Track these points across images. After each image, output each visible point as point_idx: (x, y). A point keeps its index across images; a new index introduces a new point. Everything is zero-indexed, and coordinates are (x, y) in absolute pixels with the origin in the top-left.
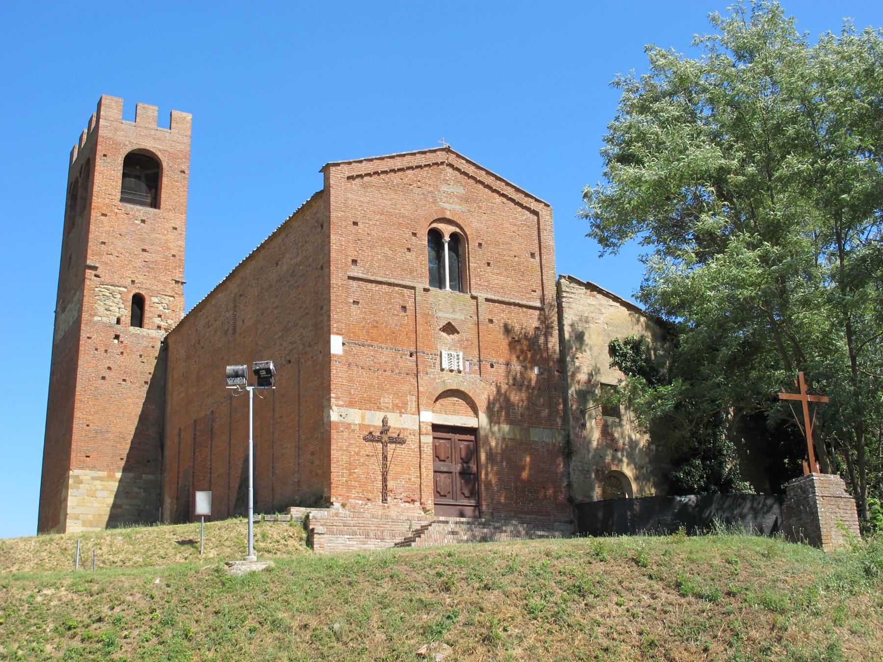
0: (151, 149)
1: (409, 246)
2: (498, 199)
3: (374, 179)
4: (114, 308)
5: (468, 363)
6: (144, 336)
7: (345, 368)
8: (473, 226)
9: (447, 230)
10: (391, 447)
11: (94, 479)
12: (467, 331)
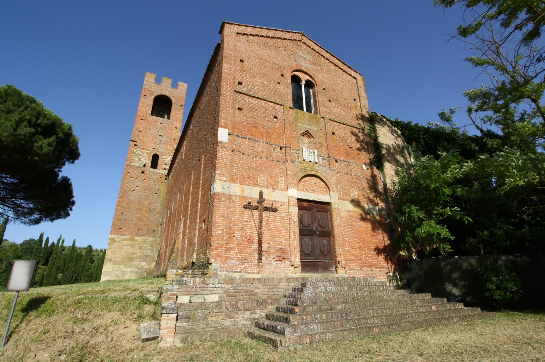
0: (169, 96)
1: (279, 81)
2: (333, 67)
3: (256, 39)
4: (143, 159)
5: (320, 158)
6: (157, 173)
7: (229, 152)
8: (320, 78)
9: (304, 78)
10: (266, 214)
11: (122, 240)
12: (319, 137)
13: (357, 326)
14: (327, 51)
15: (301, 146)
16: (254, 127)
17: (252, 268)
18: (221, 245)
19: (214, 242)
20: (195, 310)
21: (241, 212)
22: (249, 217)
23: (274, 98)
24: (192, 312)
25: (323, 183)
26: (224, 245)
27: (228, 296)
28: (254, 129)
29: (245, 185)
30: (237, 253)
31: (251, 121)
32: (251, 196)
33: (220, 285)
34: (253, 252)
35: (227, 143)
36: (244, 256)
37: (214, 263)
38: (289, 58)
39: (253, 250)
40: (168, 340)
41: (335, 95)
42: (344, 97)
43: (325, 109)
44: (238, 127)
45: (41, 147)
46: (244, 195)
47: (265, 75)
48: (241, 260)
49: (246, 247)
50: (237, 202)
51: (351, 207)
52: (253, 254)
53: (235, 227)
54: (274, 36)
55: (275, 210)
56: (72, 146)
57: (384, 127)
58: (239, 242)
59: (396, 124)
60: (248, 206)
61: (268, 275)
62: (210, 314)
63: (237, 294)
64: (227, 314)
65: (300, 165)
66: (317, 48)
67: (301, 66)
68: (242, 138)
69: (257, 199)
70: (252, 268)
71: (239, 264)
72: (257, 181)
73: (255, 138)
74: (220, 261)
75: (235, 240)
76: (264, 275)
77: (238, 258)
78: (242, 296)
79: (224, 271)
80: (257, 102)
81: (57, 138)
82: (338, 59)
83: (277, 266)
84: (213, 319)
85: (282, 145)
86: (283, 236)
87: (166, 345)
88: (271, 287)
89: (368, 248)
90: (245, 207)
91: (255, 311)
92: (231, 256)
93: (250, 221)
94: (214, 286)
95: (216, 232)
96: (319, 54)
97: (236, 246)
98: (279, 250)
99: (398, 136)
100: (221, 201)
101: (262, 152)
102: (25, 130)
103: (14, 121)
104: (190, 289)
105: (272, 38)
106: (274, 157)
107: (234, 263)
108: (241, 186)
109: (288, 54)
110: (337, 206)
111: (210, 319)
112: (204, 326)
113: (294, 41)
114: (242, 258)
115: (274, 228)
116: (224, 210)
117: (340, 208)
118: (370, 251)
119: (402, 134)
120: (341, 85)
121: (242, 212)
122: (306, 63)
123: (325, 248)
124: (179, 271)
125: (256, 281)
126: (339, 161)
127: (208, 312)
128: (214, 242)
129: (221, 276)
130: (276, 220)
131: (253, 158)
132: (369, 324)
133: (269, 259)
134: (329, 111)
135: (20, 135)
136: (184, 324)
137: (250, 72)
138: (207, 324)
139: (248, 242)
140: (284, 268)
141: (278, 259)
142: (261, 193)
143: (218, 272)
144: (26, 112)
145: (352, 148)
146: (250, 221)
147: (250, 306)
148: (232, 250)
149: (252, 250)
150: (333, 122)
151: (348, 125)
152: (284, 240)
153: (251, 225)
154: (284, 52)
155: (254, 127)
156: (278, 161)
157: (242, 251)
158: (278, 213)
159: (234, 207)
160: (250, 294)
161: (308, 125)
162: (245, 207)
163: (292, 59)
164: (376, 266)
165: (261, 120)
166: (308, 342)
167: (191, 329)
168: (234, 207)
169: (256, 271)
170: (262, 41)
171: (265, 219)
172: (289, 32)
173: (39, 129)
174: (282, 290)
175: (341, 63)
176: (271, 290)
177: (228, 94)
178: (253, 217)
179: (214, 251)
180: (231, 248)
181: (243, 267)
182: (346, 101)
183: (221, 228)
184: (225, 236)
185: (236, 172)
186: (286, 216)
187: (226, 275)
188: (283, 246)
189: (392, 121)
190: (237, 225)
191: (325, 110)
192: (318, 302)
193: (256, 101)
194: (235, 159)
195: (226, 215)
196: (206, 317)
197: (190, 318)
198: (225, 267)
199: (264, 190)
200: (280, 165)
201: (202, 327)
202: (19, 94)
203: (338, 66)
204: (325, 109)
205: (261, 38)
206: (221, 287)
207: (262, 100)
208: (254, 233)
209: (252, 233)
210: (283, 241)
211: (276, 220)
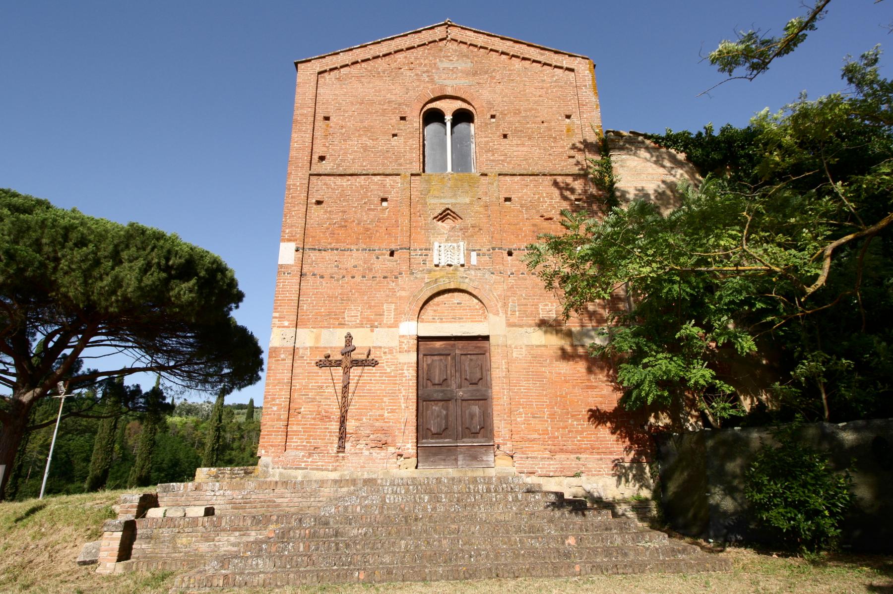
3: (354, 70)
5: (474, 254)
10: (355, 371)
13: (343, 565)
14: (502, 39)
15: (432, 239)
16: (343, 227)
17: (325, 462)
18: (277, 428)
19: (265, 425)
20: (160, 528)
21: (312, 373)
22: (326, 379)
23: (383, 165)
24: (155, 531)
25: (476, 301)
26: (280, 428)
27: (233, 508)
28: (341, 232)
29: (321, 327)
30: (302, 439)
31: (337, 218)
32: (331, 345)
33: (221, 492)
34: (330, 436)
35: (292, 266)
36: (314, 442)
37: (265, 455)
38: (419, 80)
39: (330, 432)
40: (108, 565)
41: (519, 122)
42: (539, 120)
43: (493, 155)
44: (314, 234)
45: (178, 296)
46: (319, 345)
47: (367, 129)
48: (309, 450)
49: (318, 429)
50: (307, 357)
51: (539, 337)
52: (330, 439)
53: (302, 399)
54: (388, 52)
55: (375, 364)
56: (223, 285)
57: (635, 154)
58: (306, 421)
59: (671, 141)
60: (326, 362)
61: (352, 473)
62: (179, 534)
63: (248, 505)
64: (204, 535)
65: (426, 276)
66: (481, 40)
67: (443, 87)
68: (319, 250)
69: (340, 347)
70: (325, 462)
71: (303, 456)
72: (344, 318)
73: (342, 246)
74: (273, 452)
75: (300, 419)
76: (346, 473)
77: (304, 446)
78: (255, 508)
79: (278, 468)
80: (349, 183)
81: (200, 278)
82: (529, 45)
83: (370, 458)
84: (183, 540)
85: (393, 247)
86: (387, 406)
87: (104, 571)
88: (304, 494)
89: (573, 416)
90: (320, 364)
91: (248, 532)
92: (293, 444)
93: (327, 387)
94: (213, 493)
95: (269, 408)
96: (486, 48)
97: (302, 428)
98: (376, 431)
99: (678, 164)
100: (279, 360)
101: (355, 267)
102: (152, 278)
103: (137, 270)
104: (179, 498)
105: (384, 56)
106: (377, 272)
107: (296, 456)
108: (315, 330)
109: (417, 75)
110: (501, 341)
111: (179, 541)
112: (170, 550)
113: (432, 44)
114: (311, 446)
115: (371, 393)
116: (283, 373)
117: (509, 343)
118: (578, 420)
119: (689, 158)
120: (535, 96)
121: (315, 373)
122: (456, 78)
123: (476, 419)
124: (212, 469)
125: (279, 484)
126: (515, 253)
127: (177, 531)
128: (265, 425)
129: (274, 476)
130: (375, 380)
131: (338, 280)
132: (370, 565)
133: (358, 447)
134: (502, 158)
135: (147, 286)
136: (144, 546)
137: (341, 133)
138: (175, 548)
139: (322, 419)
140: (383, 459)
141: (374, 445)
142: (349, 338)
143: (270, 470)
144: (154, 254)
145: (551, 219)
146: (327, 387)
147: (241, 524)
148: (294, 435)
149: (329, 432)
150: (508, 178)
151: (544, 175)
152: (388, 413)
153: (328, 392)
154: (409, 73)
155: (343, 227)
156: (385, 277)
157: (311, 435)
158: (380, 367)
159: (301, 366)
160: (268, 506)
161: (451, 197)
162: (320, 364)
163: (424, 81)
164: (592, 450)
165: (356, 213)
166: (221, 584)
167: (152, 552)
168: (301, 366)
169: (333, 466)
170: (366, 69)
171: (353, 379)
172: (420, 32)
173: (173, 272)
174: (324, 499)
175: (538, 50)
176: (305, 500)
177: (298, 184)
178: (333, 379)
179: (264, 438)
180: (293, 431)
181: (310, 460)
182: (545, 124)
183: (277, 402)
184: (283, 414)
185: (307, 310)
186: (394, 370)
187: (281, 474)
188: (386, 422)
189: (659, 138)
190: (304, 395)
191: (491, 158)
192: (331, 523)
193: (348, 180)
194: (307, 289)
195: (286, 381)
196: (173, 539)
197: (151, 538)
198: (280, 461)
199: (354, 332)
200: (388, 283)
201: (167, 550)
202: (143, 232)
203: (529, 59)
204: (493, 155)
205: (363, 64)
206: (224, 495)
207: (360, 175)
208: (333, 405)
209: (330, 405)
210: (386, 414)
211: (375, 380)
